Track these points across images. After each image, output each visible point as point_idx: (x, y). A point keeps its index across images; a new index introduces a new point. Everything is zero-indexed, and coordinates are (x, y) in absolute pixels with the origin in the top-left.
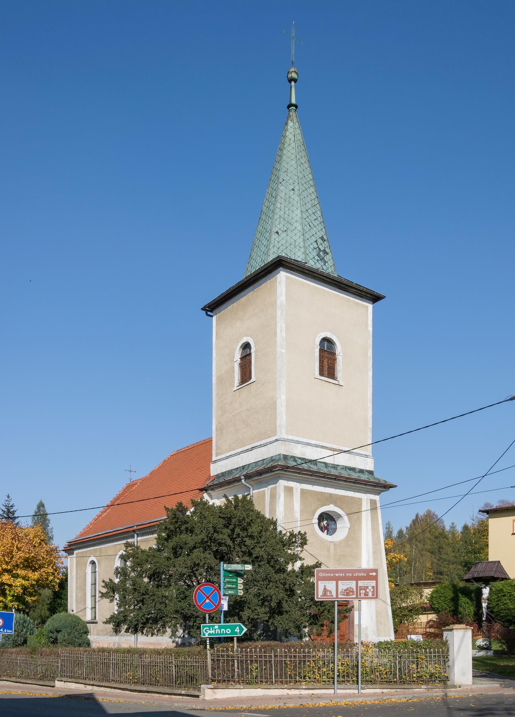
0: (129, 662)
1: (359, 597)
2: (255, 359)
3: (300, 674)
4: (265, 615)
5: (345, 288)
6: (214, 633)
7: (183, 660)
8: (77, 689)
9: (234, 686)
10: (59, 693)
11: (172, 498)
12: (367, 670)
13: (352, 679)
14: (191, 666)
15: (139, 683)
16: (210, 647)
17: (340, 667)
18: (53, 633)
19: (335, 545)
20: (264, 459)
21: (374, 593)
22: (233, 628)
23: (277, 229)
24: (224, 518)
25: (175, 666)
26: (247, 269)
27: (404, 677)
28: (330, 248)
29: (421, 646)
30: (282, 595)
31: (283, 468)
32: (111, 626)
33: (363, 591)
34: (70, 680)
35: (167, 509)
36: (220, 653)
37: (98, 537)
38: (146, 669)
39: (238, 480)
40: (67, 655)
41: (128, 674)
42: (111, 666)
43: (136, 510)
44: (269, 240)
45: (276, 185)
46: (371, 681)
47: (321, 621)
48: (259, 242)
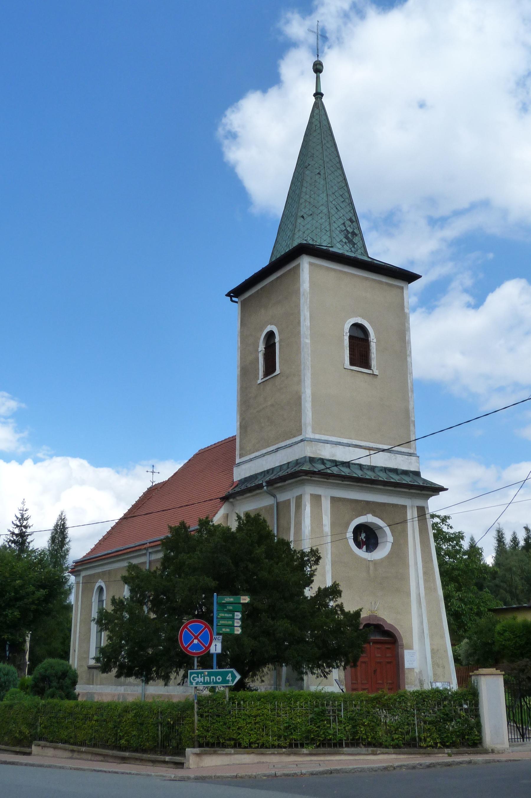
23: (302, 214)
44: (295, 225)
45: (302, 170)
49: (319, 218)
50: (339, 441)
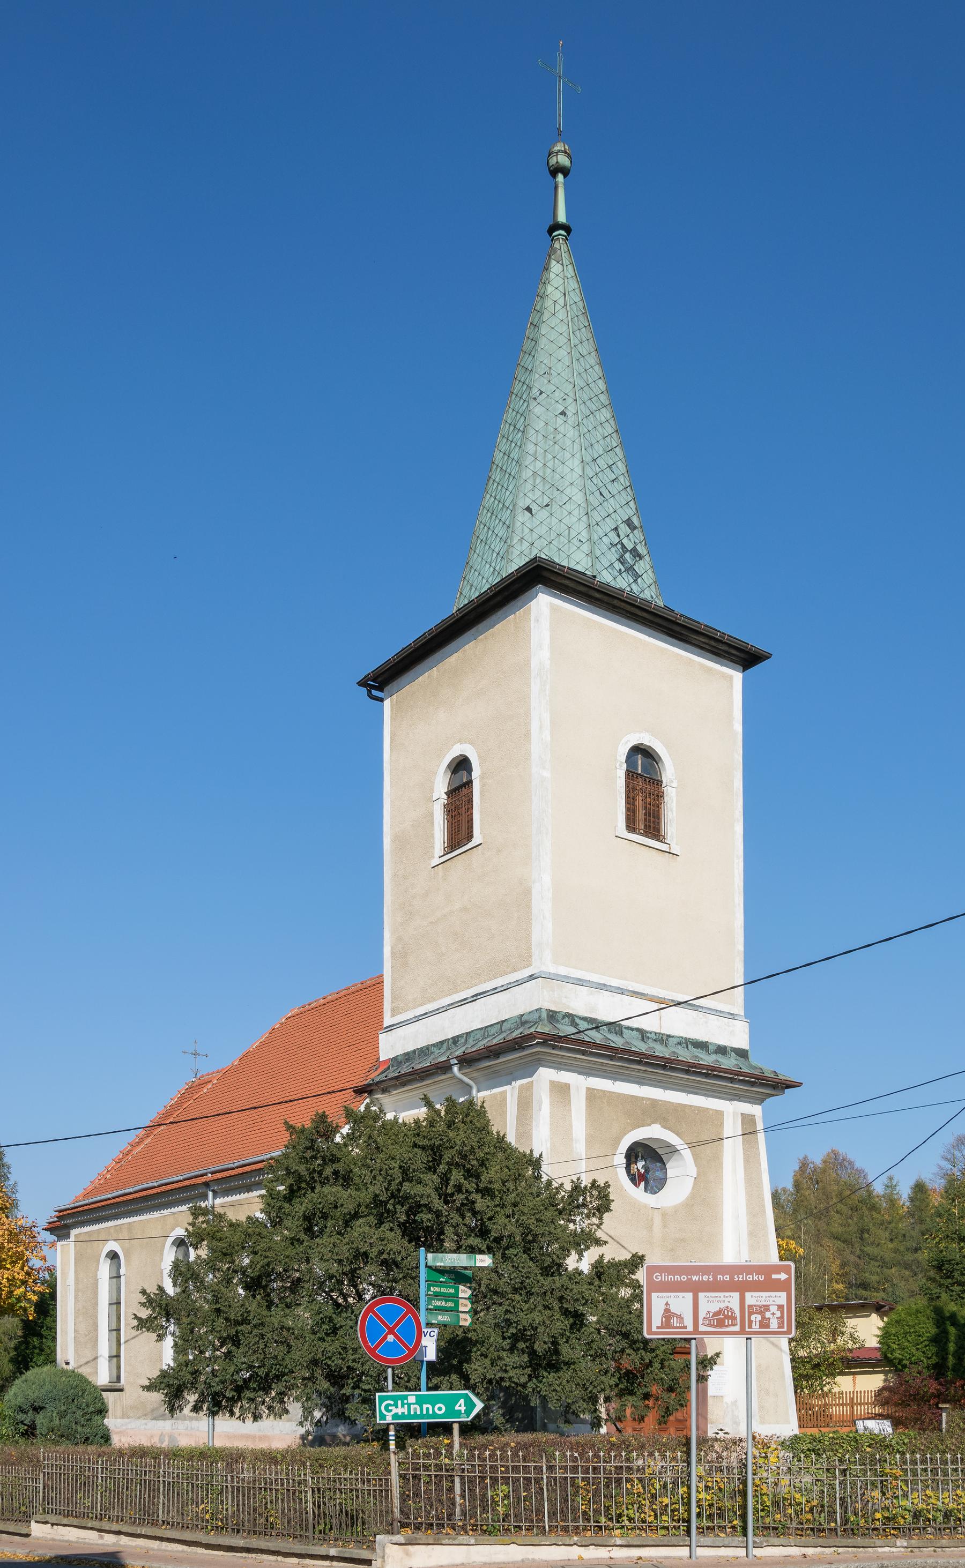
0: (203, 1481)
1: (747, 1329)
2: (481, 793)
3: (608, 1509)
4: (519, 1371)
5: (681, 634)
6: (406, 1413)
7: (332, 1475)
8: (81, 1543)
9: (454, 1539)
10: (40, 1552)
11: (292, 1111)
12: (765, 1502)
13: (730, 1522)
14: (352, 1490)
15: (227, 1528)
16: (397, 1447)
17: (703, 1495)
18: (26, 1413)
19: (664, 1215)
20: (503, 1022)
21: (783, 1322)
22: (453, 1401)
23: (528, 502)
24: (423, 1148)
25: (313, 1491)
26: (461, 593)
27: (852, 1519)
28: (646, 544)
29: (891, 1446)
30: (561, 1324)
31: (546, 1041)
32: (157, 1397)
33: (755, 1315)
34: (65, 1521)
35: (290, 1128)
36: (421, 1461)
37: (124, 1198)
38: (244, 1495)
39: (444, 1068)
40: (58, 1463)
41: (201, 1508)
42: (161, 1490)
43: (211, 1137)
45: (526, 404)
46: (775, 1529)
47: (645, 1386)
48: (488, 531)
49: (565, 513)
50: (603, 982)
